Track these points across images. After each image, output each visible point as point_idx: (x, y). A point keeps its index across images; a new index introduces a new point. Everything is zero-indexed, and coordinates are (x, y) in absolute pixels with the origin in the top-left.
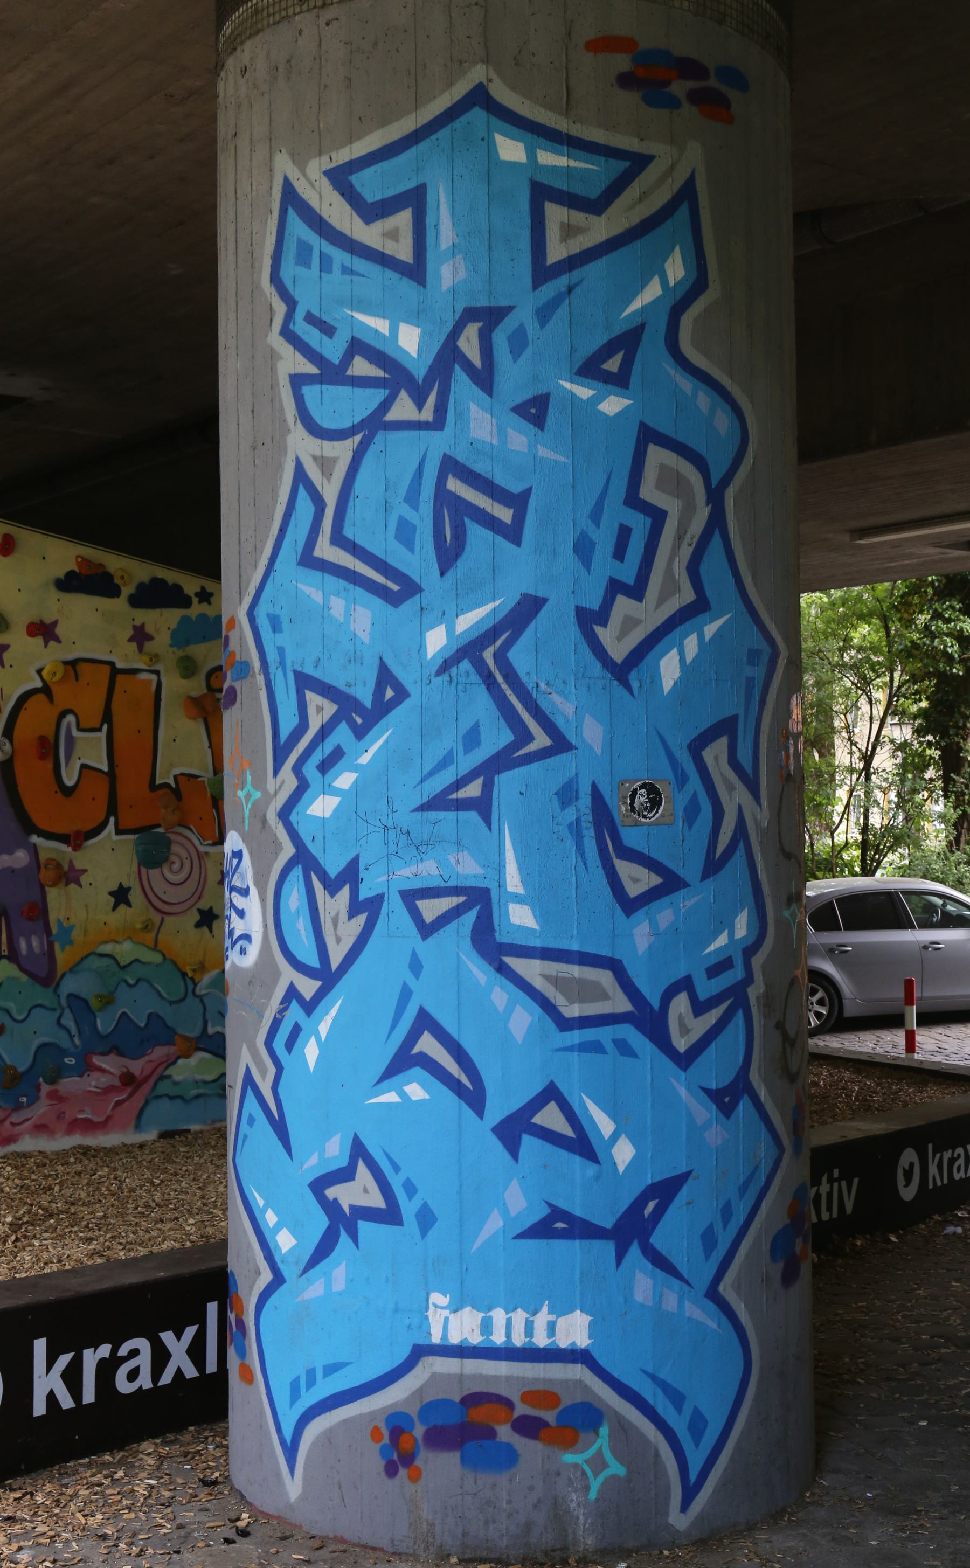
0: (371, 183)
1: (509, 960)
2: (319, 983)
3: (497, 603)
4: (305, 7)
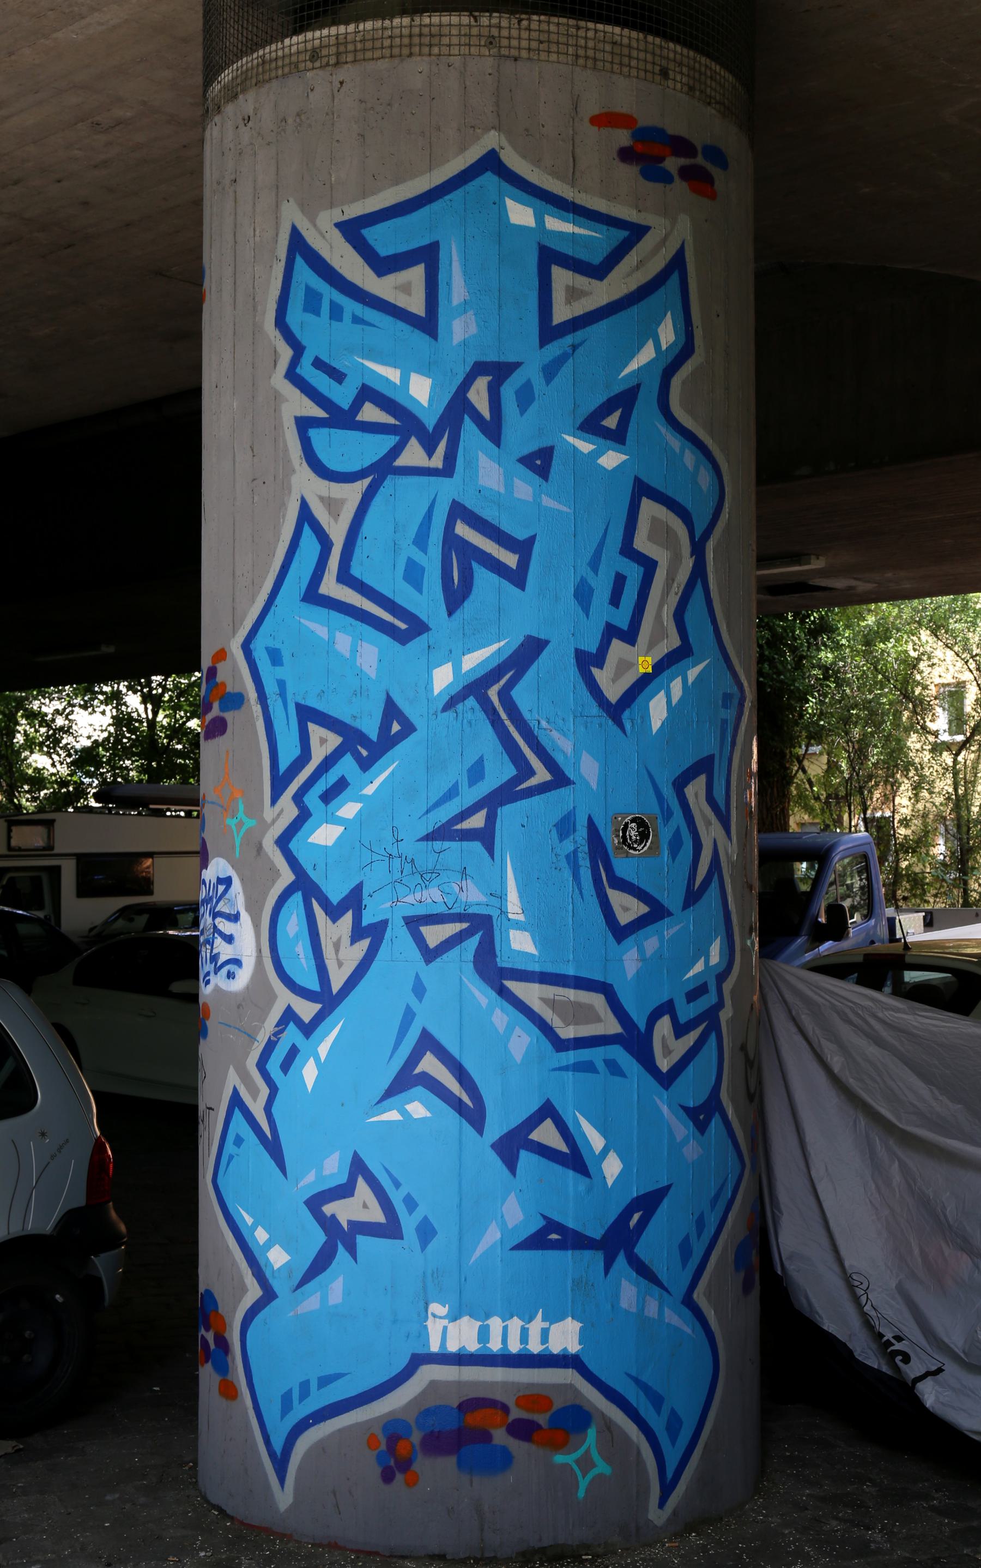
0: (384, 238)
1: (510, 984)
2: (319, 1006)
3: (502, 643)
4: (317, 64)
